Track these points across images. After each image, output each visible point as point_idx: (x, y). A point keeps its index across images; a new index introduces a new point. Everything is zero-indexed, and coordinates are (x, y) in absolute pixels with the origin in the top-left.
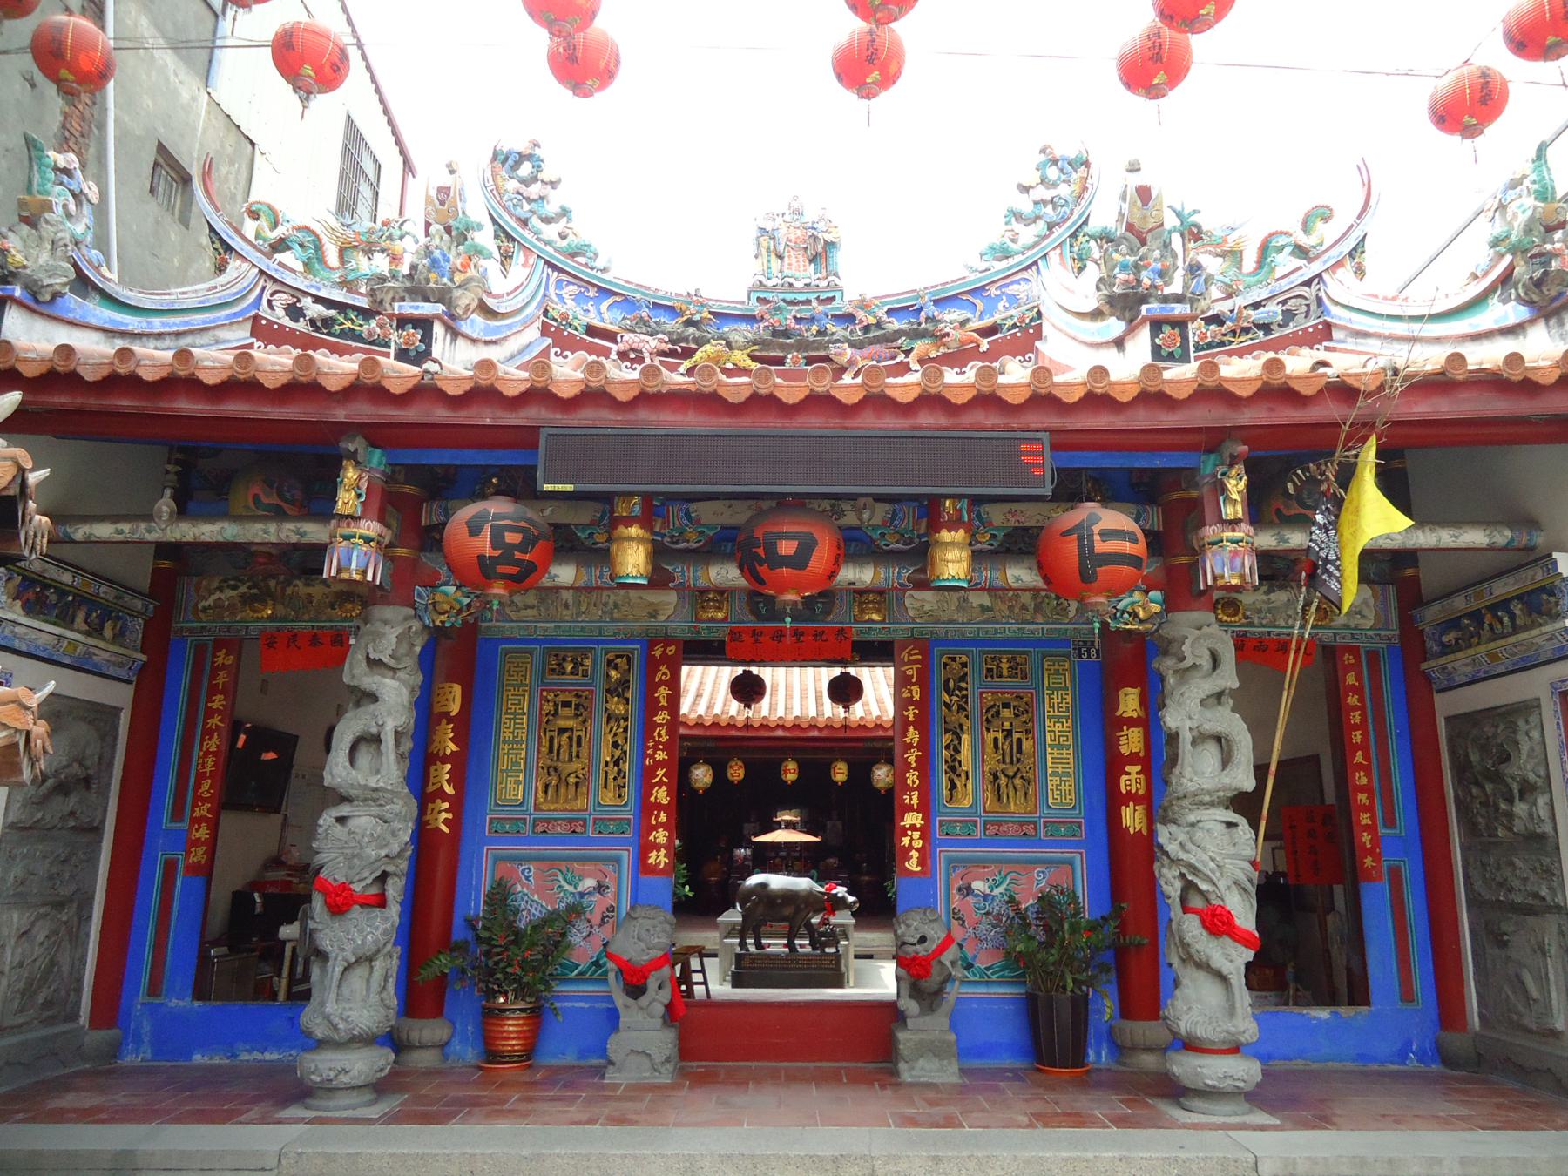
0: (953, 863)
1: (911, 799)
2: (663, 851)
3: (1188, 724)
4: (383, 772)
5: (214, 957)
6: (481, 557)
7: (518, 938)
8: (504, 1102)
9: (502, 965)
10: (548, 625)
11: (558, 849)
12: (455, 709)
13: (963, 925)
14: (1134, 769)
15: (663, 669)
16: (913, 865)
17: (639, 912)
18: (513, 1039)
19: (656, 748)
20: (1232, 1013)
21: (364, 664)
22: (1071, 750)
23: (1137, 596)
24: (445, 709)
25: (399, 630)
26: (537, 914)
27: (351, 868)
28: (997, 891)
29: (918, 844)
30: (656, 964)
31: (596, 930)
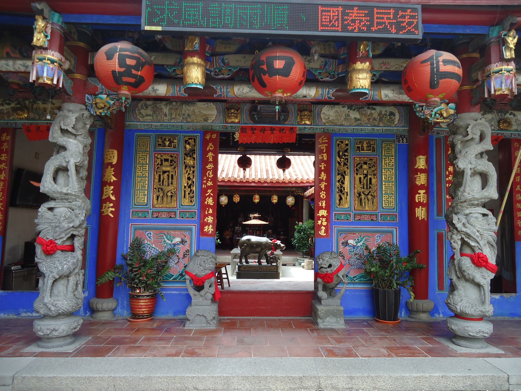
0: (340, 232)
1: (322, 204)
2: (211, 226)
3: (470, 166)
4: (70, 185)
5: (13, 270)
6: (114, 72)
7: (146, 262)
8: (135, 341)
9: (138, 276)
10: (157, 124)
11: (351, 227)
12: (115, 161)
13: (344, 259)
14: (422, 192)
15: (211, 144)
16: (322, 233)
17: (200, 253)
18: (144, 308)
19: (207, 180)
20: (483, 303)
21: (59, 132)
22: (393, 183)
23: (443, 106)
24: (110, 161)
25: (76, 115)
26: (155, 253)
27: (55, 233)
28: (359, 244)
29: (325, 223)
30: (208, 277)
31: (181, 260)
